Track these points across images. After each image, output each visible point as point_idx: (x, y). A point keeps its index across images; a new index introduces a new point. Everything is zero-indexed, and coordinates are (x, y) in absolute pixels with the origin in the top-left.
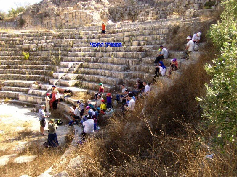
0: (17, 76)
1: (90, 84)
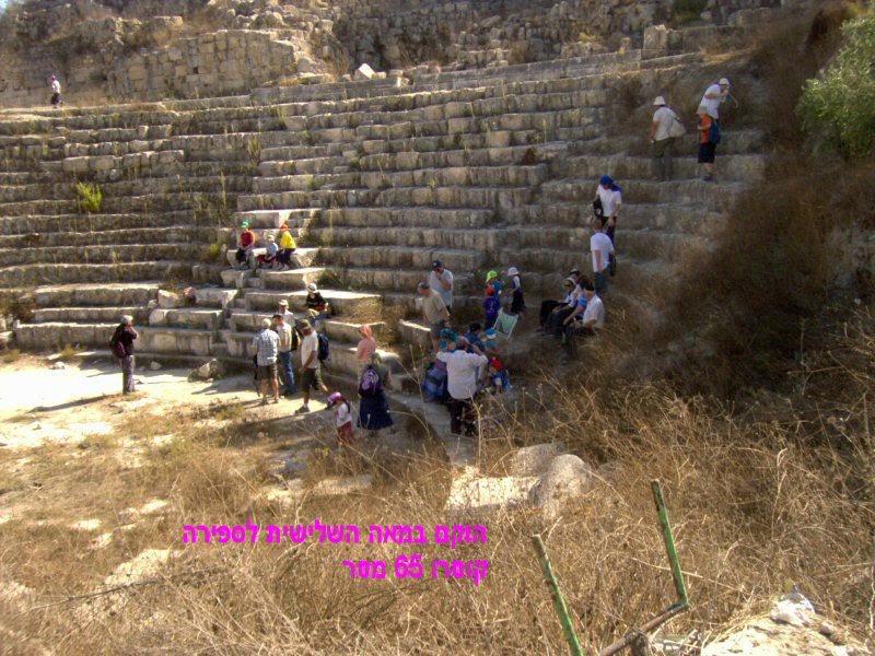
0: (74, 272)
1: (381, 276)
